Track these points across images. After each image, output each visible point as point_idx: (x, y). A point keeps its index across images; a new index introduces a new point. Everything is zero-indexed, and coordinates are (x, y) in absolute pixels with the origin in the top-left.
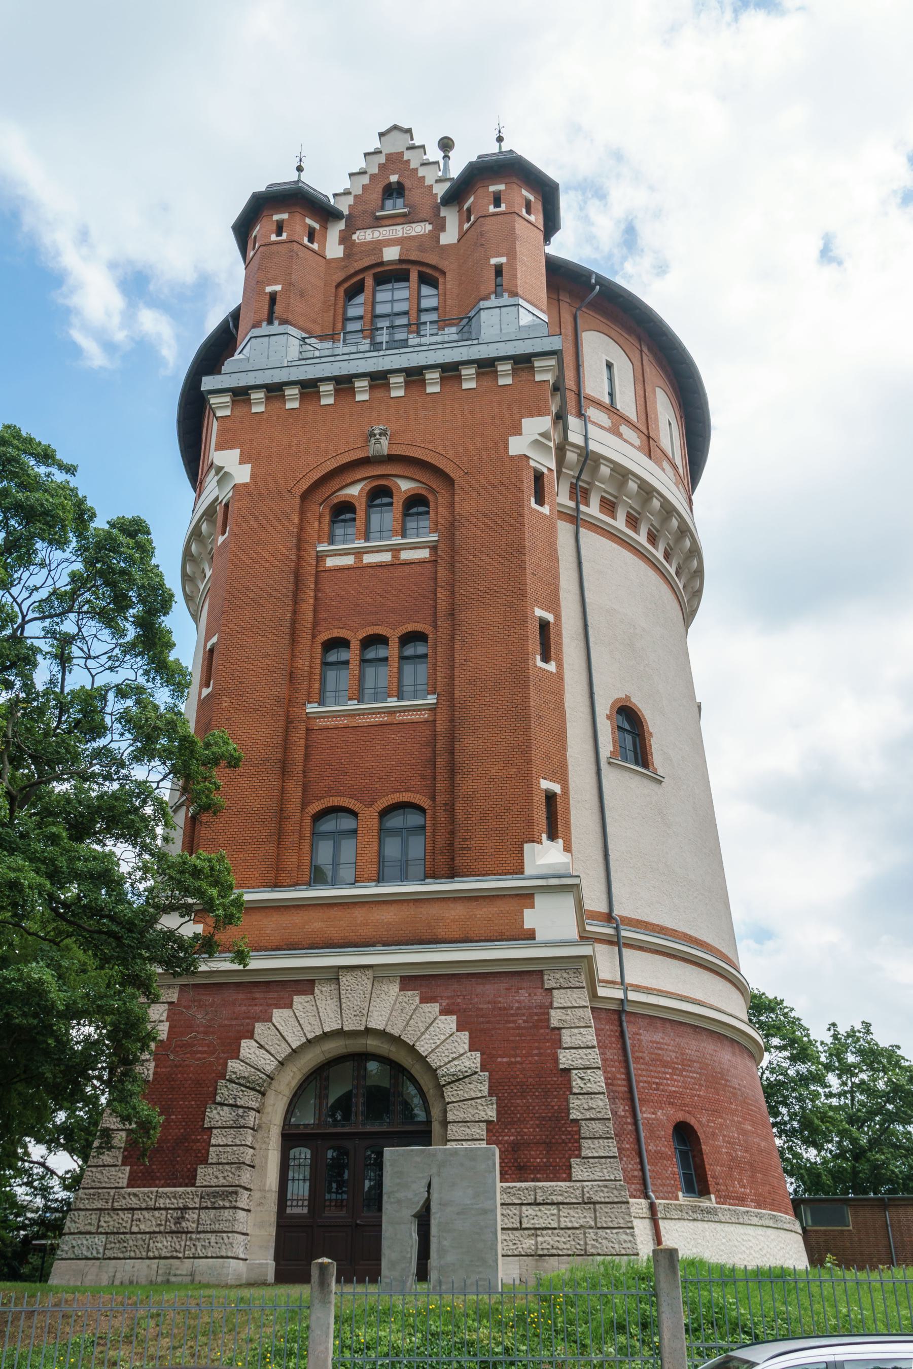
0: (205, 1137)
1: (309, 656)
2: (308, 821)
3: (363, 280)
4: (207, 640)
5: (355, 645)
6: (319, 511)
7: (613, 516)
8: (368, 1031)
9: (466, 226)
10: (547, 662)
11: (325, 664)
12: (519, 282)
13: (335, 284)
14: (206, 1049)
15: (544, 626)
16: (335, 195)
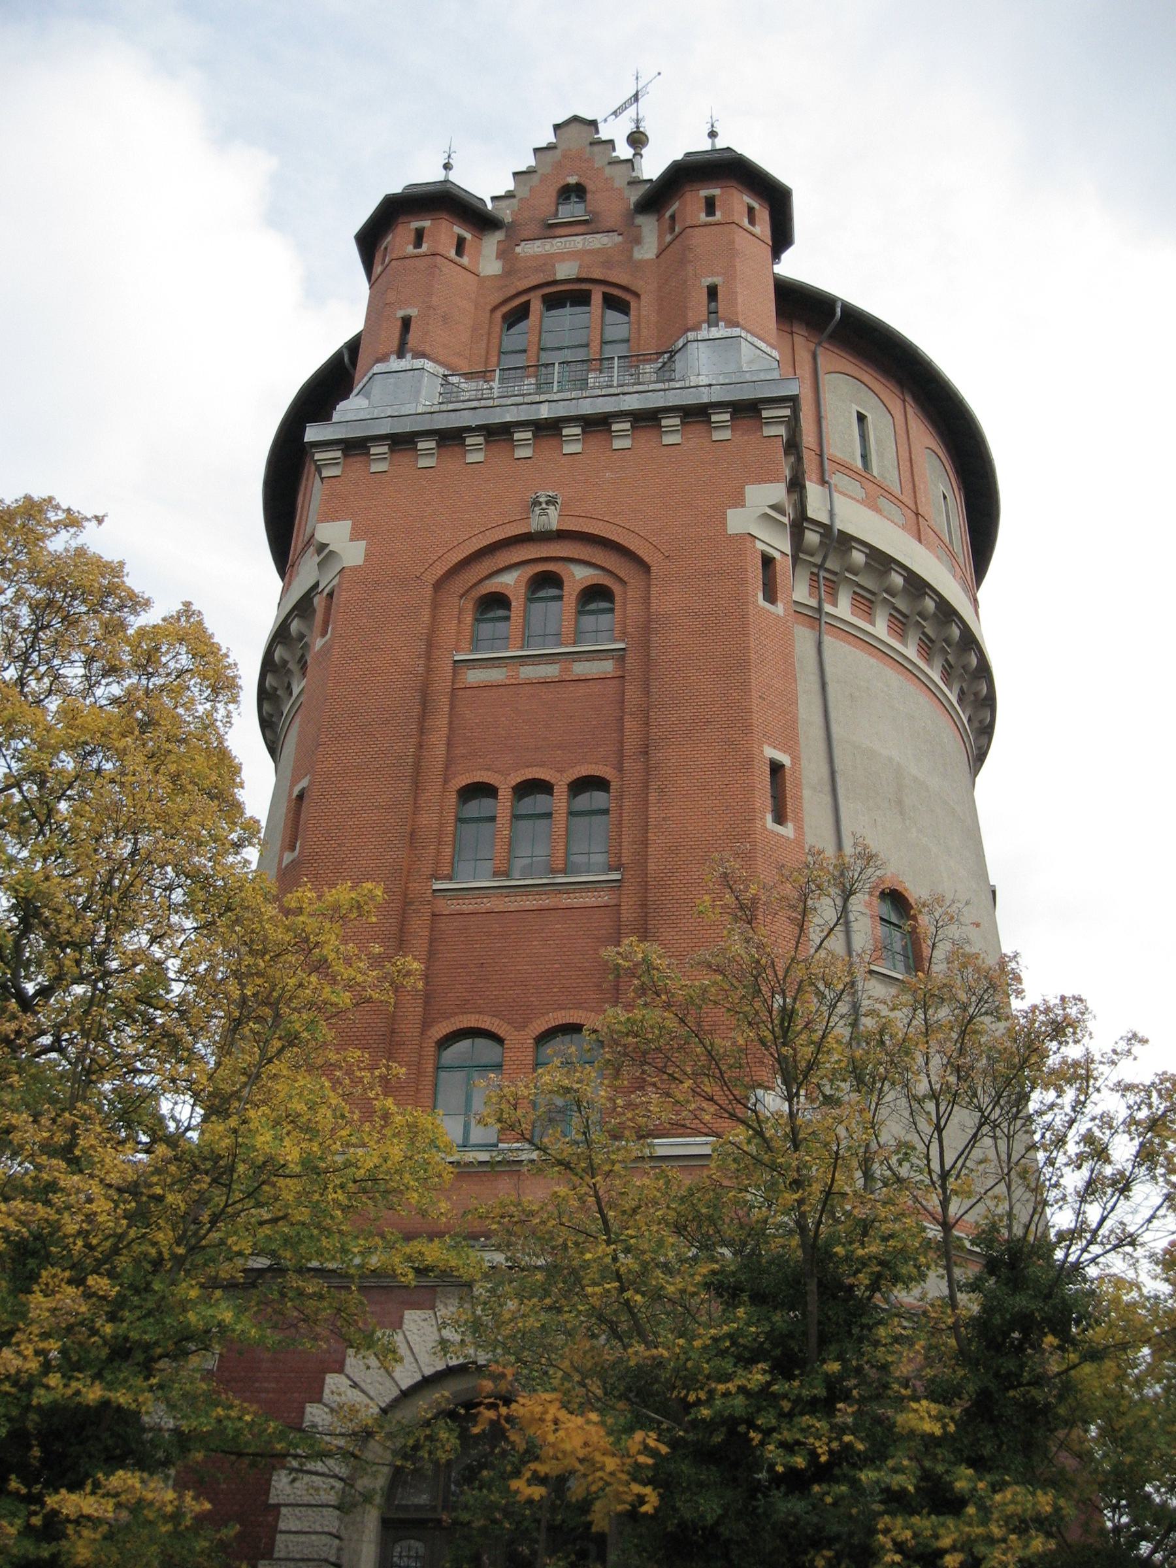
0: (270, 1519)
1: (439, 805)
2: (430, 1049)
3: (527, 303)
4: (294, 783)
5: (505, 793)
6: (458, 615)
7: (870, 617)
9: (669, 238)
10: (780, 823)
11: (460, 820)
12: (739, 308)
13: (489, 308)
14: (273, 1385)
15: (776, 769)
16: (494, 199)
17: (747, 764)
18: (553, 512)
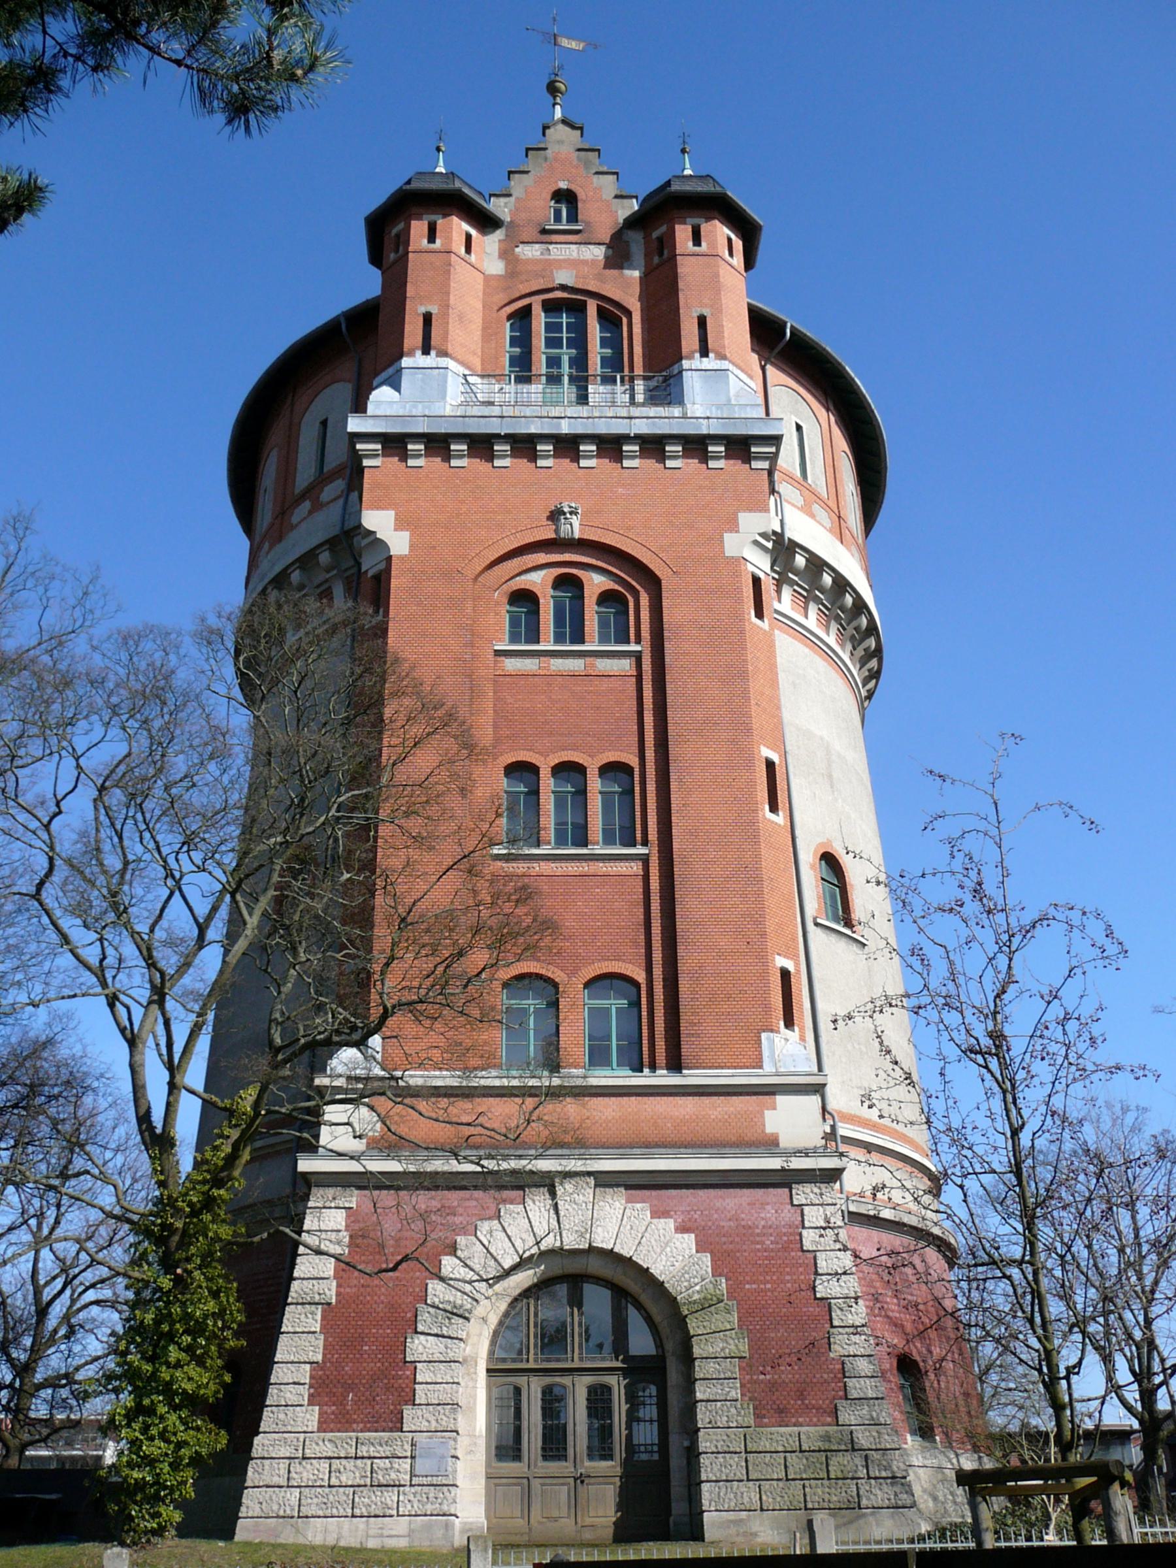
0: (408, 1373)
8: (592, 1250)
12: (726, 342)
17: (749, 763)
18: (576, 521)
